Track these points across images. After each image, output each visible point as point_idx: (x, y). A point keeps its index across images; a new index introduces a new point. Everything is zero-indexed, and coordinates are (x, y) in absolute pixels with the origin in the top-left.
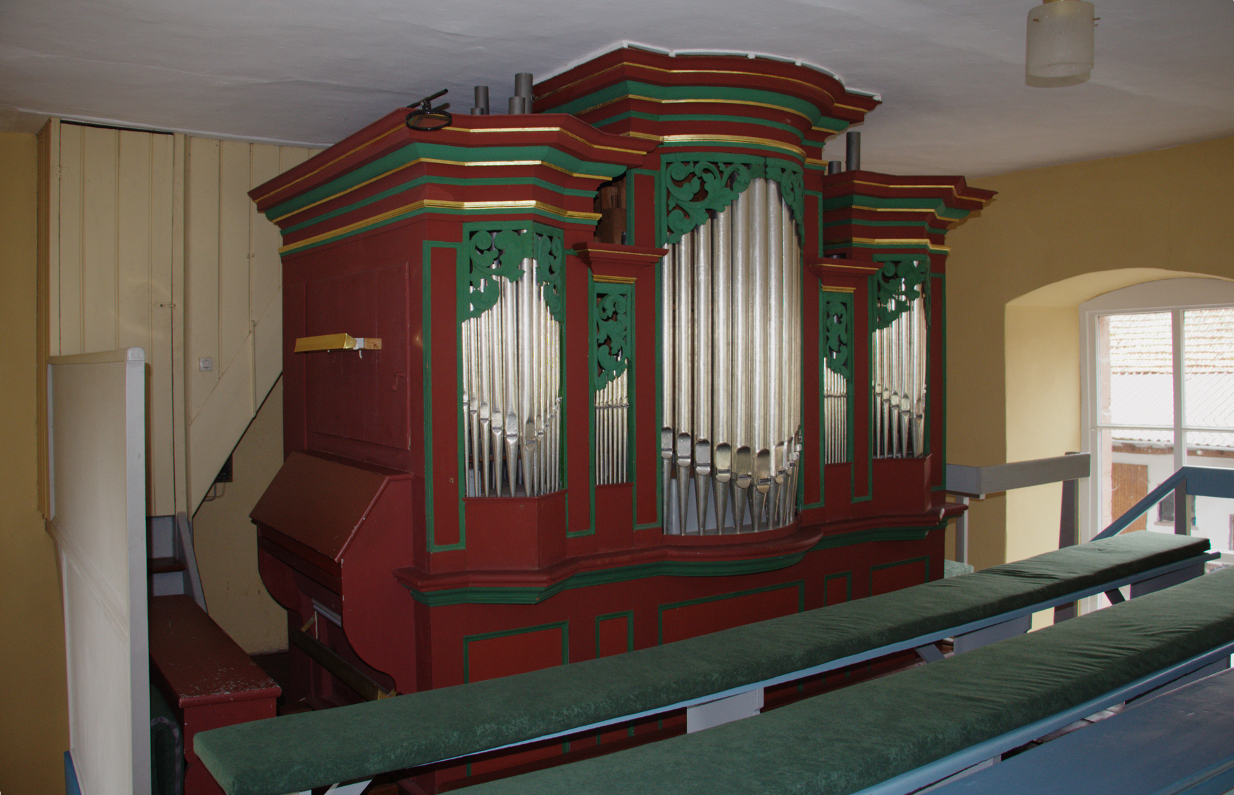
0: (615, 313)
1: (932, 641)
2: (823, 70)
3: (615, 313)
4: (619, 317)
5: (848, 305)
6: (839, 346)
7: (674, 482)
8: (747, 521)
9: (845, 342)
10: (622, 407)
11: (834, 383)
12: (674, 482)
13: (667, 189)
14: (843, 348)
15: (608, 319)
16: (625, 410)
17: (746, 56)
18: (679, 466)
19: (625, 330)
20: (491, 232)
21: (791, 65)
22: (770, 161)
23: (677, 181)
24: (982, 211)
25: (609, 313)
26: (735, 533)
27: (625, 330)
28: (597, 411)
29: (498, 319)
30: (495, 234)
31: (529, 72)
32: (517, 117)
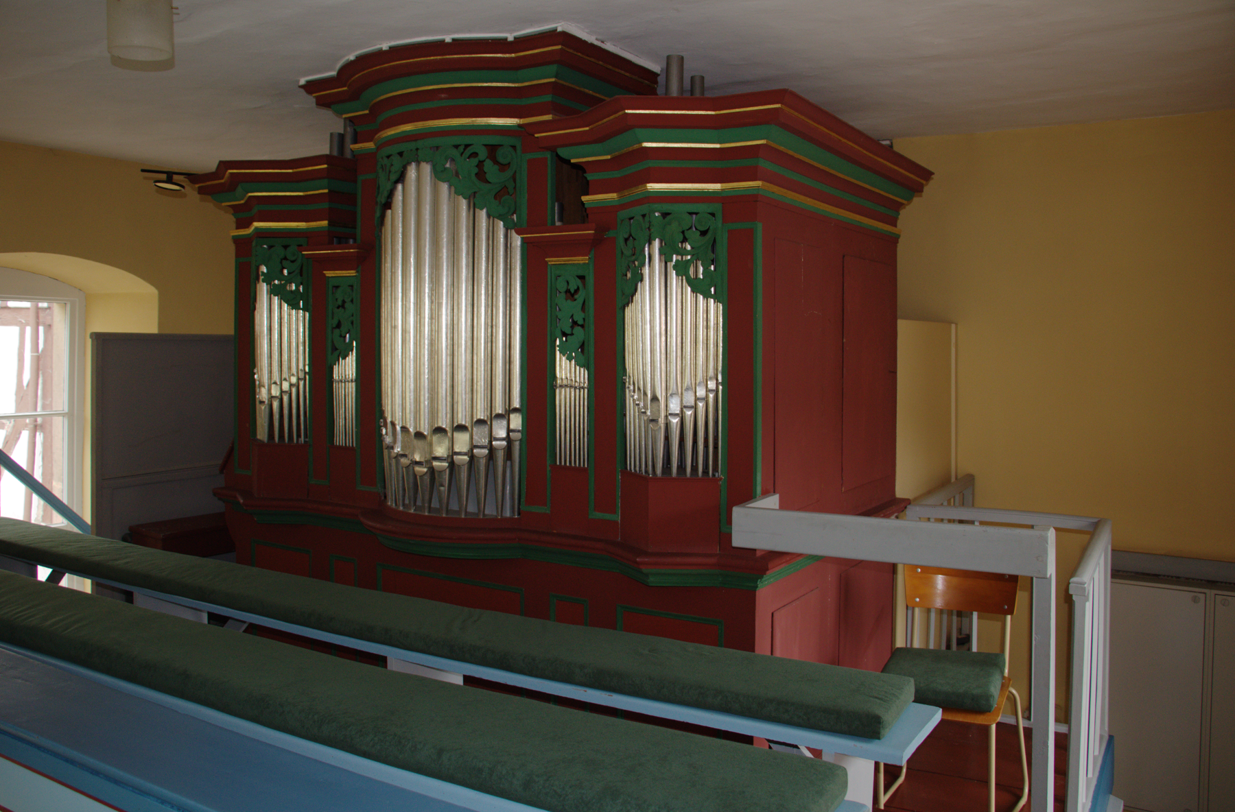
0: (344, 302)
1: (1072, 731)
2: (532, 32)
3: (344, 302)
4: (346, 305)
5: (355, 287)
6: (572, 327)
7: (509, 463)
8: (435, 504)
9: (580, 322)
10: (583, 388)
11: (566, 369)
12: (509, 463)
13: (515, 172)
14: (577, 330)
15: (338, 307)
16: (586, 390)
17: (444, 41)
18: (496, 449)
19: (353, 316)
20: (691, 214)
21: (442, 42)
22: (420, 144)
23: (502, 165)
24: (197, 193)
25: (340, 302)
26: (423, 514)
27: (353, 316)
28: (557, 391)
29: (671, 302)
30: (694, 216)
31: (681, 54)
32: (673, 98)
